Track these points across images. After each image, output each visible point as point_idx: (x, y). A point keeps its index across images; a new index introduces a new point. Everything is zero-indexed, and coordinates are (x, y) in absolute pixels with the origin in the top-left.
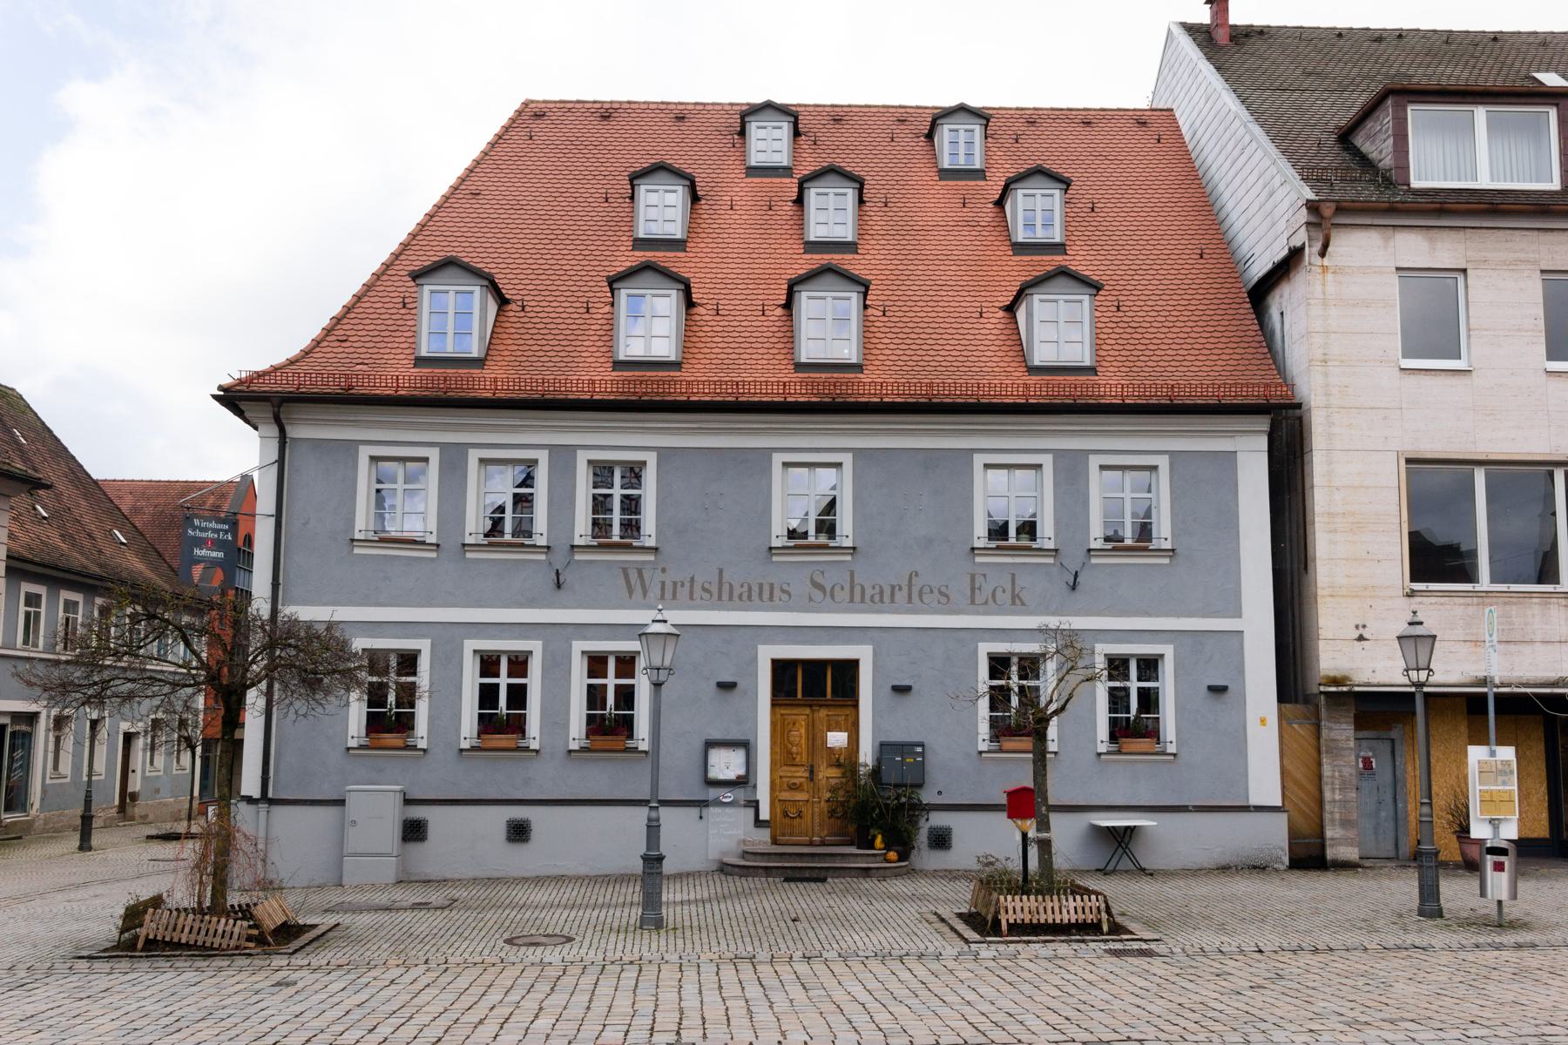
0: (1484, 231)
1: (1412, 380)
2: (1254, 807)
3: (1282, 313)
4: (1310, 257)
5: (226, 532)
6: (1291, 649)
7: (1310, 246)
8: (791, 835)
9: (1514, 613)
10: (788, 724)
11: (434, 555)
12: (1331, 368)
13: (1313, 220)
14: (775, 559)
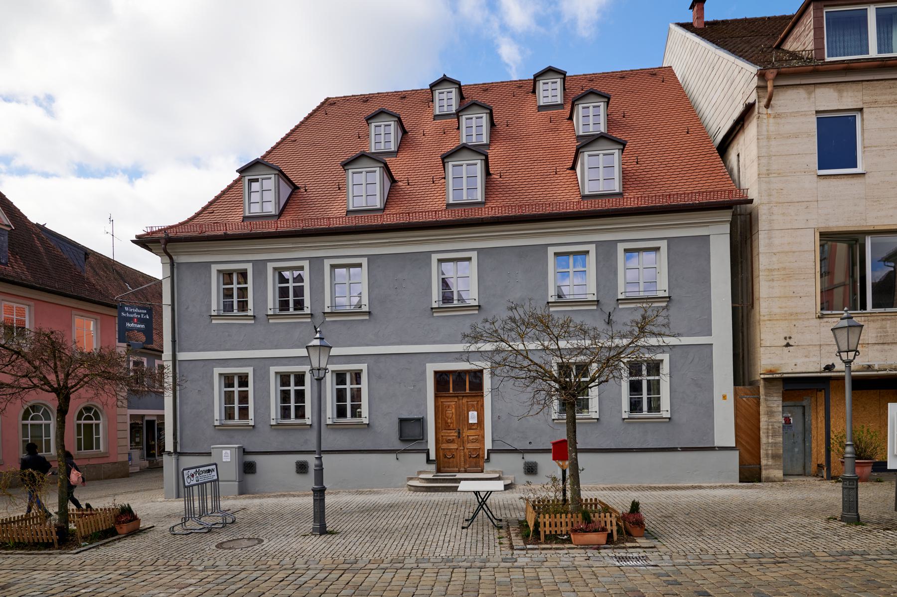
0: (875, 82)
1: (825, 182)
2: (718, 447)
3: (738, 155)
4: (759, 109)
5: (145, 314)
6: (741, 356)
7: (758, 102)
8: (448, 467)
9: (888, 325)
10: (446, 407)
11: (253, 322)
12: (772, 179)
13: (762, 84)
14: (435, 315)
